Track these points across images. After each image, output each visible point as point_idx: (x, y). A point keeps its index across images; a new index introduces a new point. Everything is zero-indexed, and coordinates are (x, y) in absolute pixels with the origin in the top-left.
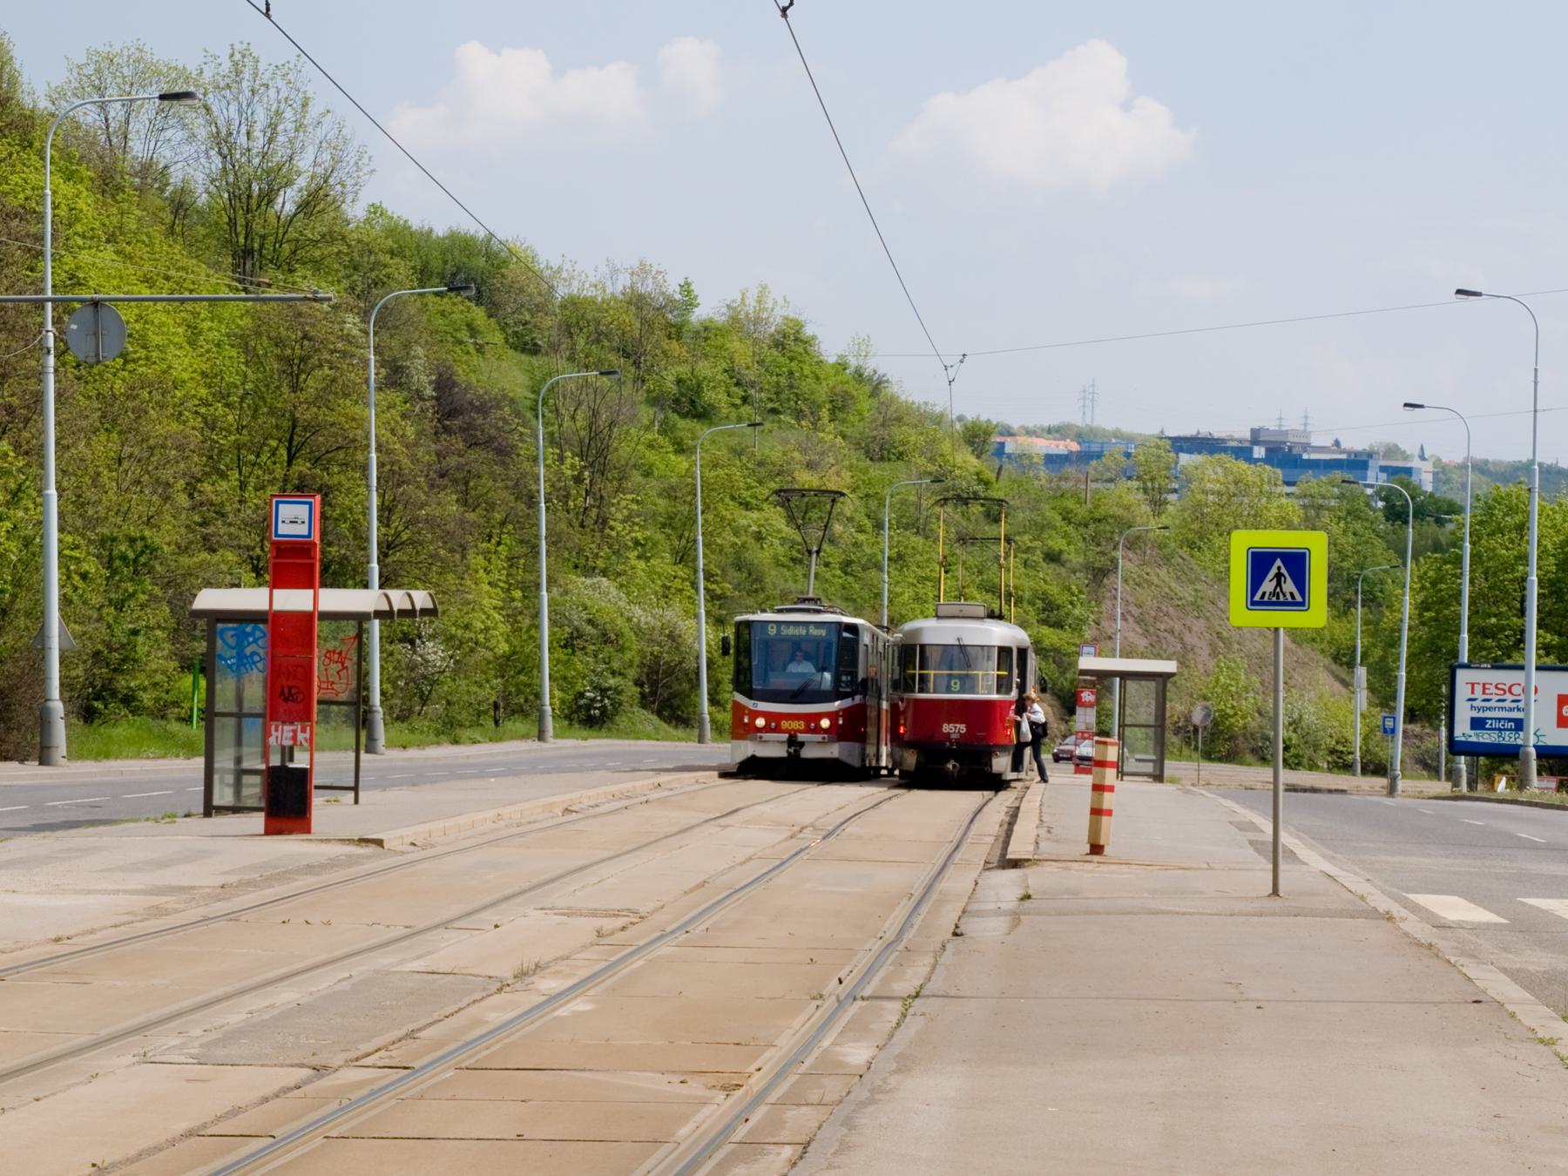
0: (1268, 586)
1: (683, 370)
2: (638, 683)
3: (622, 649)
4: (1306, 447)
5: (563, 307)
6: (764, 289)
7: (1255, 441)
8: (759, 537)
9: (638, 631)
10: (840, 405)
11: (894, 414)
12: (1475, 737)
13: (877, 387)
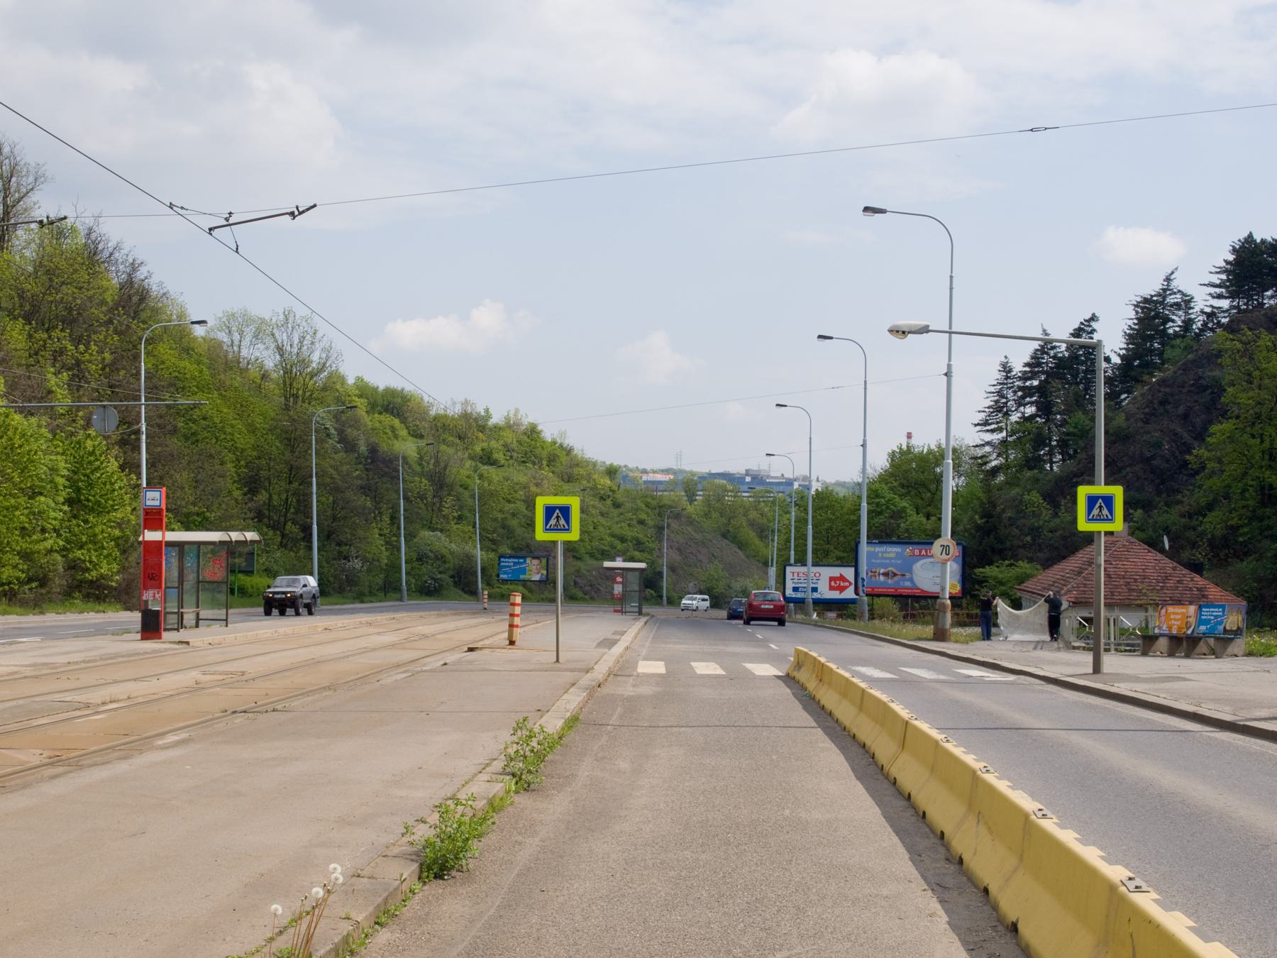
0: (553, 522)
1: (485, 445)
2: (452, 577)
3: (445, 562)
4: (768, 477)
5: (435, 418)
6: (517, 411)
7: (747, 474)
8: (514, 515)
9: (452, 553)
10: (552, 459)
11: (577, 463)
12: (794, 595)
13: (569, 451)
